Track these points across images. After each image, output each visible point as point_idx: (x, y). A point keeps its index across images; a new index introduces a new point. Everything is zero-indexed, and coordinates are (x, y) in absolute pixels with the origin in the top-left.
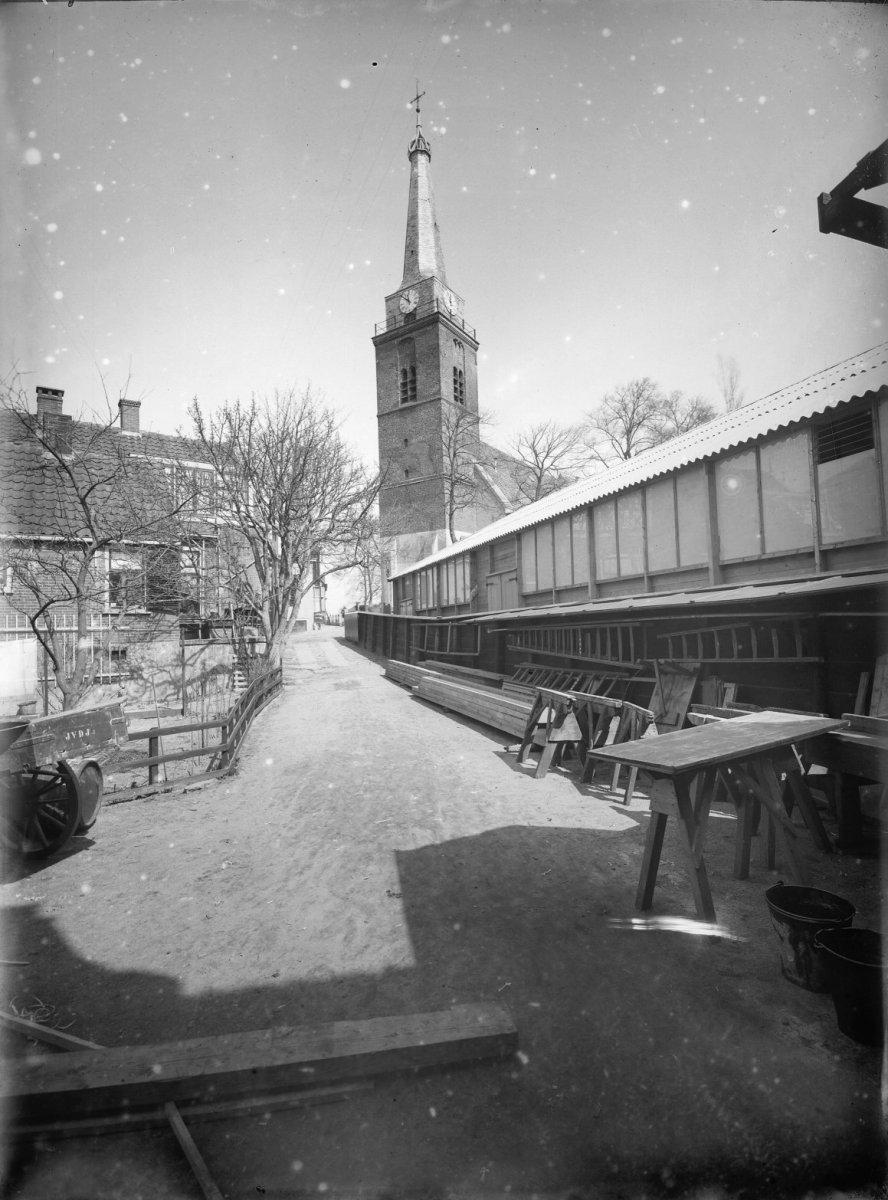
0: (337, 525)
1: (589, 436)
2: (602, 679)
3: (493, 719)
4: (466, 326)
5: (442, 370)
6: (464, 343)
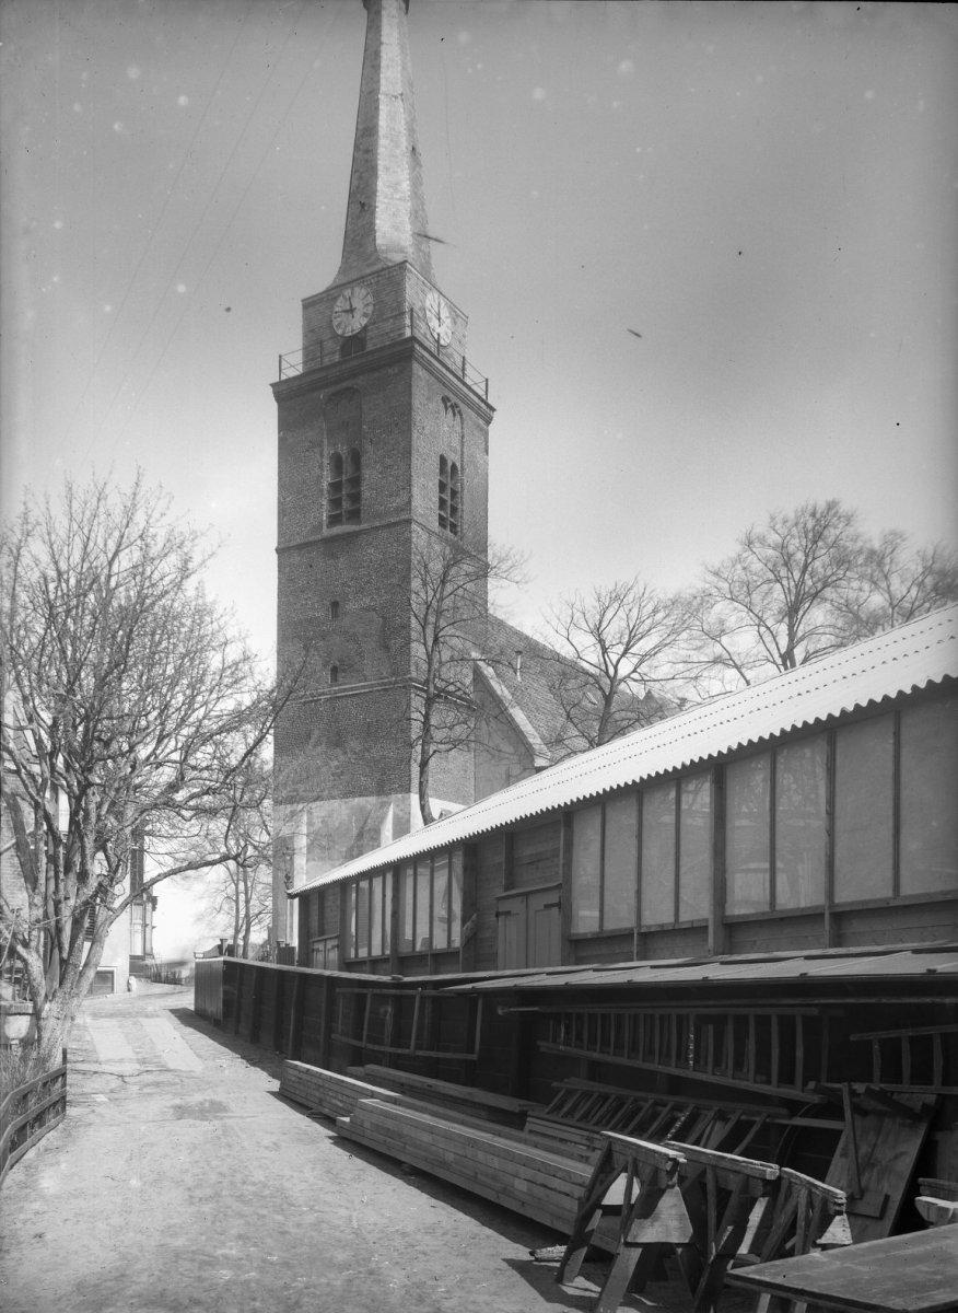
0: (191, 774)
1: (711, 617)
2: (734, 1119)
3: (507, 1191)
4: (469, 371)
5: (416, 461)
6: (462, 405)
